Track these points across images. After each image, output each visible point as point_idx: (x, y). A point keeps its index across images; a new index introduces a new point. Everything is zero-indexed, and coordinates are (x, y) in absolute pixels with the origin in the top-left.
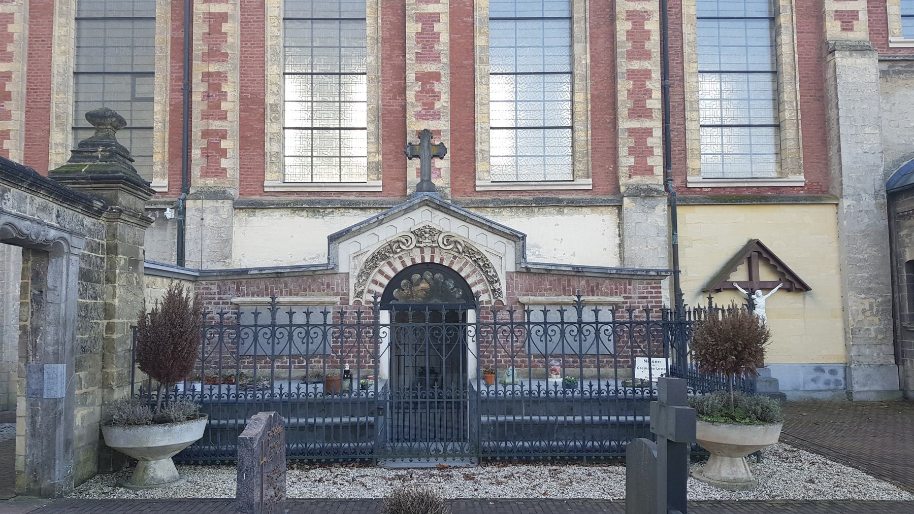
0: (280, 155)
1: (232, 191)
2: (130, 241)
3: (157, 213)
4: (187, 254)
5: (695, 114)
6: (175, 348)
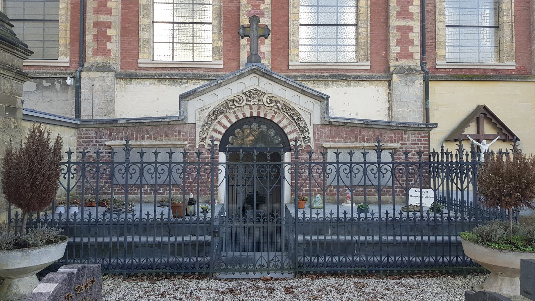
0: (150, 42)
1: (115, 66)
2: (7, 91)
3: (61, 81)
4: (82, 110)
5: (442, 17)
6: (34, 182)
